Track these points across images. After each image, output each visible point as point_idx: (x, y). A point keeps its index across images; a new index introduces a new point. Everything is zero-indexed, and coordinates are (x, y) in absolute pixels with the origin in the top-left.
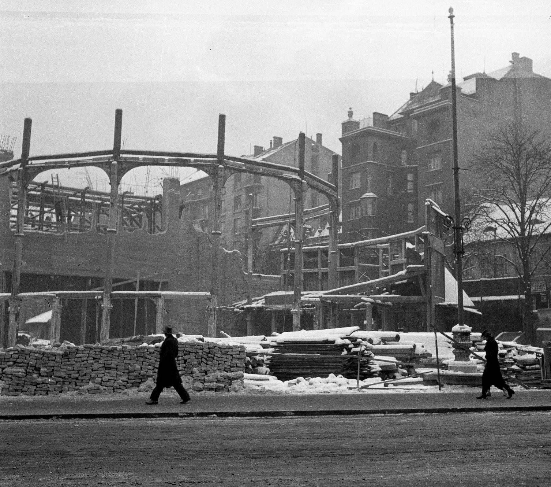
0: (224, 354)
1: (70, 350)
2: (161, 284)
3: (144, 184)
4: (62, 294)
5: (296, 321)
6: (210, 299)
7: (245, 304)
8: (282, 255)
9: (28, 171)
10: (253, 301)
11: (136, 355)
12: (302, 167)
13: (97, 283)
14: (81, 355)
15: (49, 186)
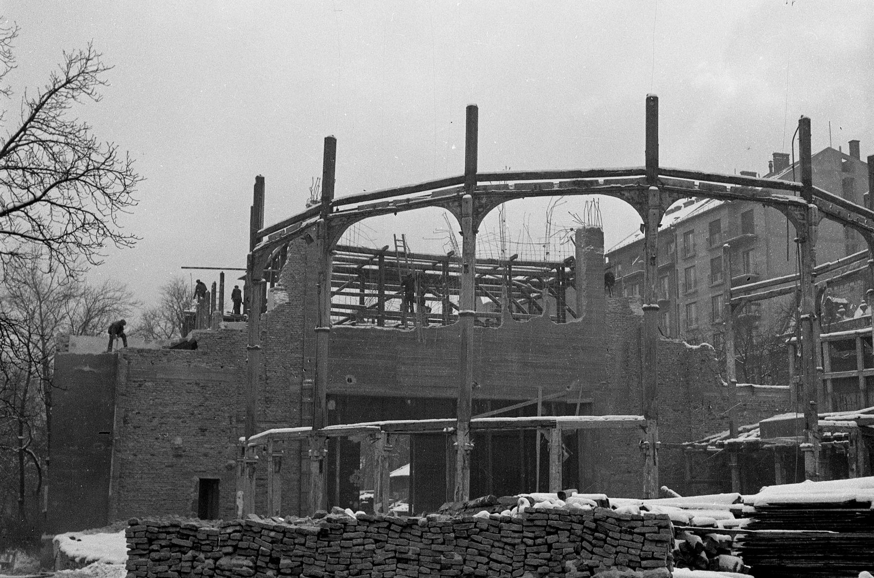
0: (626, 532)
1: (333, 525)
3: (543, 241)
4: (391, 425)
5: (810, 463)
6: (644, 428)
7: (726, 438)
8: (791, 350)
9: (333, 224)
10: (741, 432)
11: (452, 535)
12: (807, 181)
13: (448, 407)
14: (352, 535)
15: (391, 254)
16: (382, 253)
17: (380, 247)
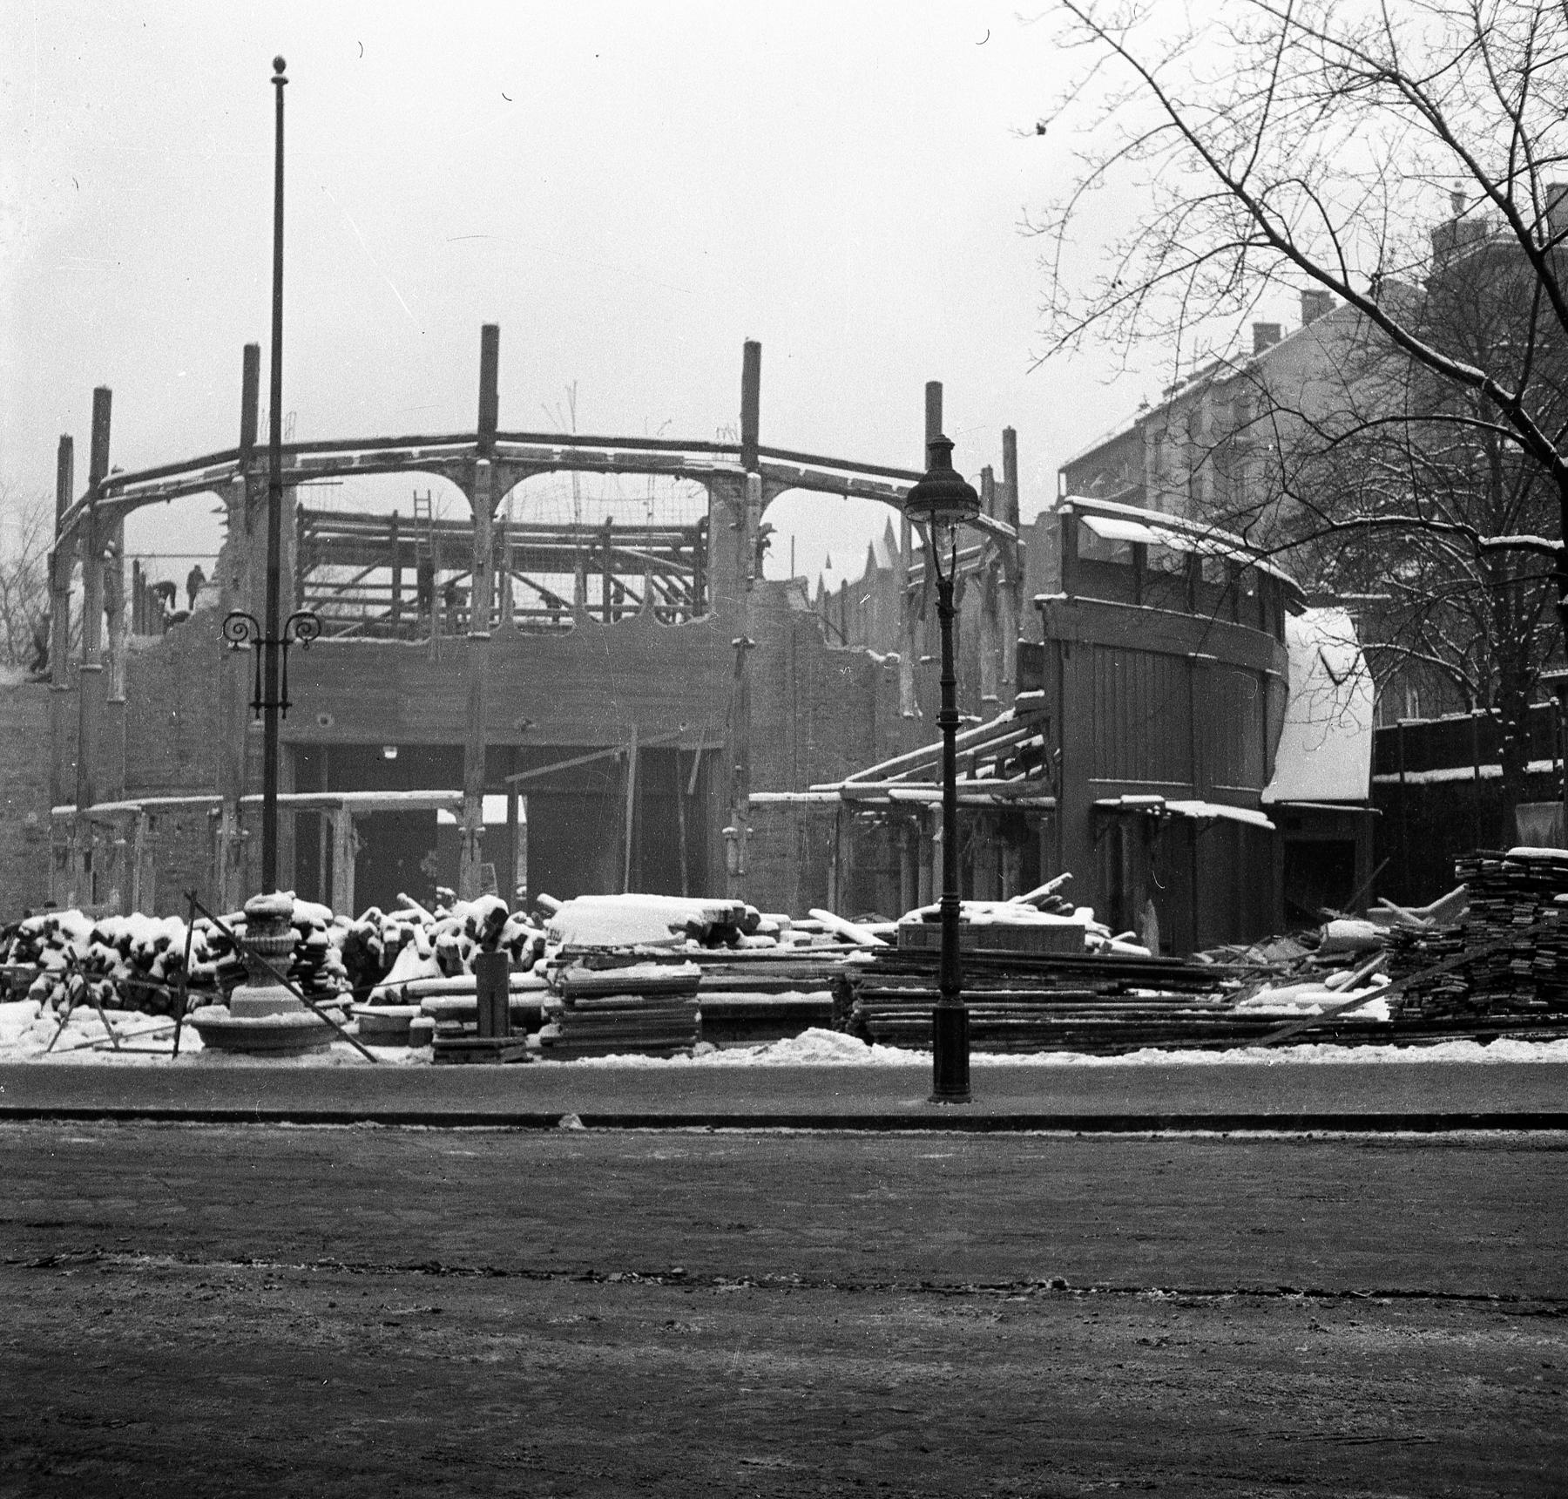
2: (698, 755)
4: (153, 805)
16: (394, 521)
17: (390, 513)
